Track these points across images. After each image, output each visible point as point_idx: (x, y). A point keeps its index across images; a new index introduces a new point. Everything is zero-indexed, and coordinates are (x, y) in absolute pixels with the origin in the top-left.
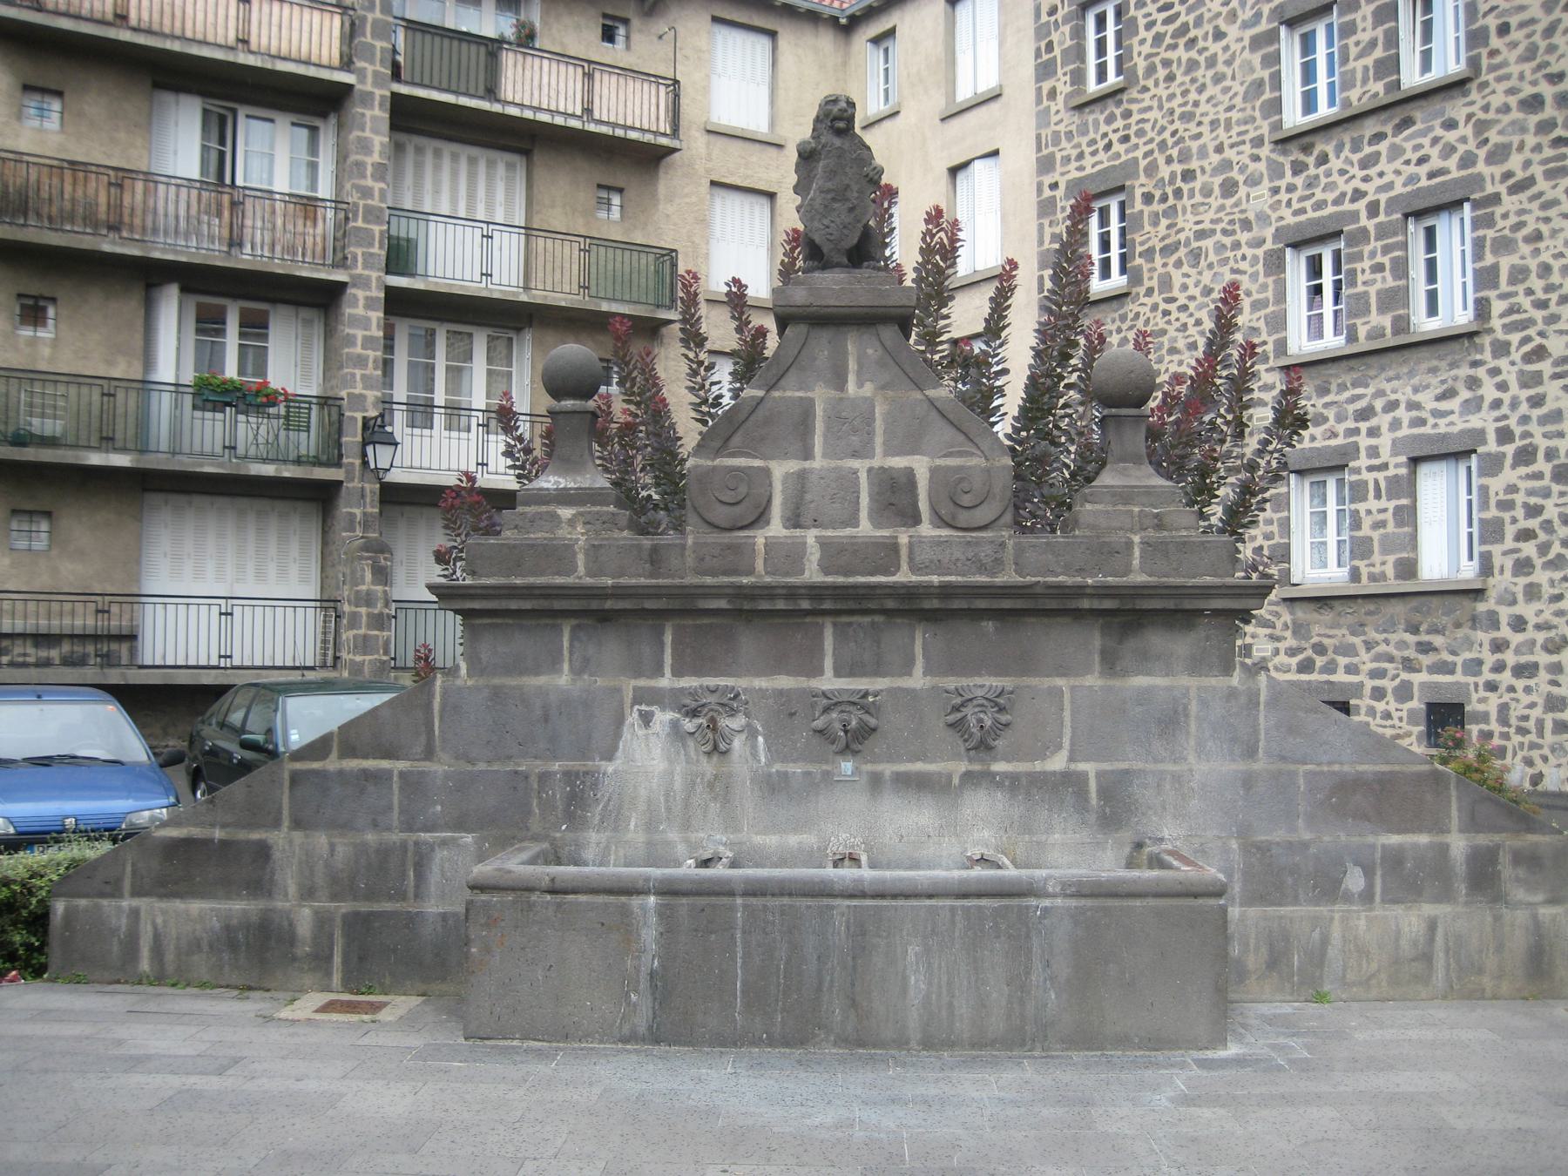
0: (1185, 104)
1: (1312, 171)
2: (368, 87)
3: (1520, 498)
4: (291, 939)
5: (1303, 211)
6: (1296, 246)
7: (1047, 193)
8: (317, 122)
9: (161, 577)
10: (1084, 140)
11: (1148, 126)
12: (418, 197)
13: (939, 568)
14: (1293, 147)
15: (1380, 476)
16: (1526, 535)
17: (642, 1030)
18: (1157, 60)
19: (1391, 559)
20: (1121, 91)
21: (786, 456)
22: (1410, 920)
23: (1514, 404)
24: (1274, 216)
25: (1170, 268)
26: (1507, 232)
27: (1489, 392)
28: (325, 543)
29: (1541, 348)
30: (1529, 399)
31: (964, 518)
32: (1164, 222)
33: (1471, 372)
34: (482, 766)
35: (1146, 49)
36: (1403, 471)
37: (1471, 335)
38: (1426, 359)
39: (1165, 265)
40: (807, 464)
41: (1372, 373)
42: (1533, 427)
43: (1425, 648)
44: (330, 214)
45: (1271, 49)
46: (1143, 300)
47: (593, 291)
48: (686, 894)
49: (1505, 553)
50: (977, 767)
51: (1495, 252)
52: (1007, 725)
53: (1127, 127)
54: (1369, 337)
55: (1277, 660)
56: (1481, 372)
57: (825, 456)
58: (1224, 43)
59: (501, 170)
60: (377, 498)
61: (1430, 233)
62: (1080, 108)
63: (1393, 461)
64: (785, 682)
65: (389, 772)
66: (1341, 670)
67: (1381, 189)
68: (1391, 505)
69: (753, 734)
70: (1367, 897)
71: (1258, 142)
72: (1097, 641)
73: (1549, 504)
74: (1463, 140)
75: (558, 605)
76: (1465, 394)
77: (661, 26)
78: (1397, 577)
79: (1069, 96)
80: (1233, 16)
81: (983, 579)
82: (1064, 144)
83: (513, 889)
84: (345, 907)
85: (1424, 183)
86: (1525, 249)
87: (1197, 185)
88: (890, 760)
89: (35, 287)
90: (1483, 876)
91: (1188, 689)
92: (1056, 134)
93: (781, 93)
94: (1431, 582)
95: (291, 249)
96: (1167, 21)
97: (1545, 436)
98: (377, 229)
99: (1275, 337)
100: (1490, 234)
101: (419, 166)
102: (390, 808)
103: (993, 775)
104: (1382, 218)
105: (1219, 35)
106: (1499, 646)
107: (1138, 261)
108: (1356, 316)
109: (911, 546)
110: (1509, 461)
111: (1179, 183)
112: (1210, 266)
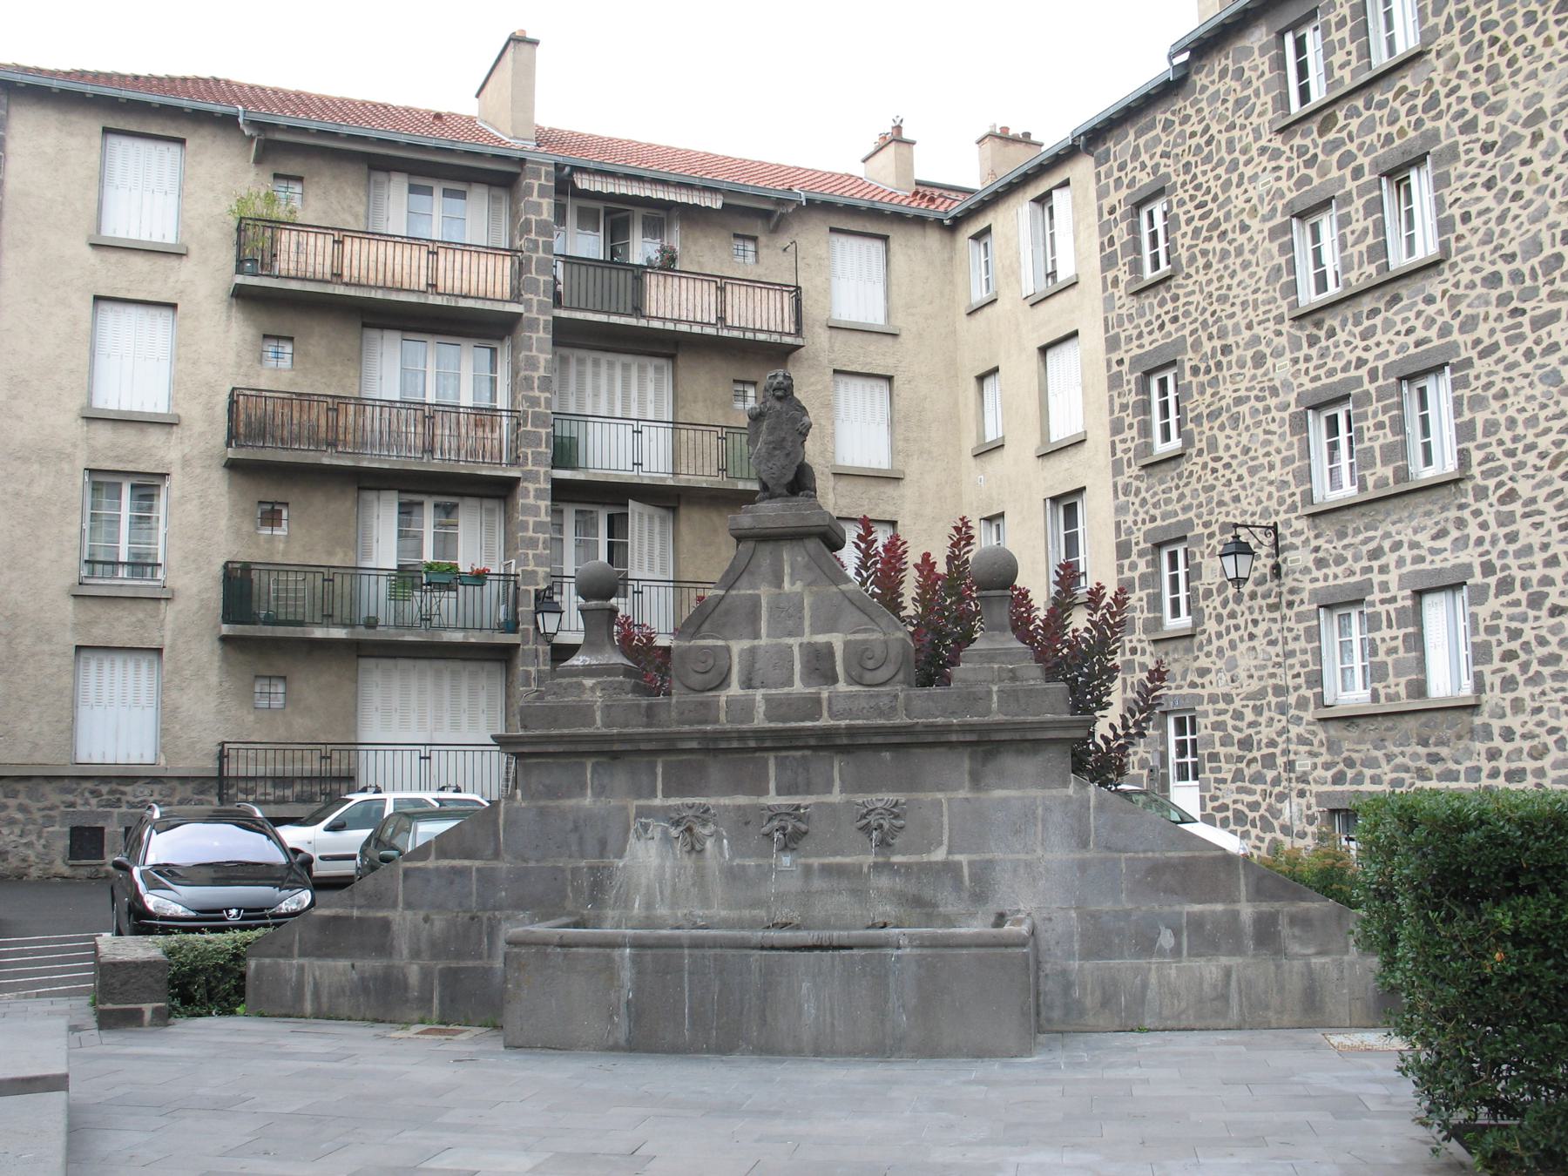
0: (1221, 288)
1: (1323, 343)
2: (534, 315)
5: (1318, 378)
6: (1316, 408)
7: (1115, 368)
8: (495, 344)
9: (373, 728)
10: (1142, 322)
11: (1192, 308)
12: (580, 402)
13: (848, 714)
14: (1307, 322)
15: (1391, 607)
16: (1509, 656)
17: (622, 1041)
18: (1196, 250)
19: (1403, 681)
20: (1170, 278)
21: (741, 637)
22: (1210, 969)
23: (1494, 542)
24: (1295, 383)
25: (1216, 431)
26: (1479, 391)
27: (1473, 531)
28: (508, 696)
29: (1512, 490)
30: (1506, 536)
31: (868, 677)
32: (1209, 391)
33: (1459, 514)
34: (532, 864)
35: (1188, 241)
36: (1409, 603)
37: (1456, 481)
38: (1422, 503)
39: (1211, 429)
40: (756, 642)
41: (1380, 517)
42: (1510, 560)
43: (1434, 758)
44: (505, 421)
46: (1195, 460)
47: (731, 473)
48: (650, 947)
49: (1494, 673)
50: (880, 859)
51: (1471, 409)
53: (1176, 309)
54: (1376, 487)
55: (1315, 774)
56: (1466, 514)
58: (1248, 234)
59: (651, 373)
60: (548, 657)
62: (1137, 293)
63: (1400, 594)
64: (742, 800)
66: (1367, 780)
67: (1378, 357)
68: (1401, 633)
69: (719, 840)
70: (1176, 952)
71: (1279, 319)
72: (966, 764)
73: (1526, 627)
74: (1441, 313)
76: (1455, 534)
77: (784, 240)
78: (1408, 697)
79: (1129, 283)
80: (1254, 210)
82: (1127, 325)
83: (536, 944)
84: (441, 965)
85: (1412, 351)
86: (1495, 405)
87: (1233, 357)
88: (817, 855)
89: (274, 494)
90: (1266, 933)
92: (1120, 316)
93: (894, 288)
95: (473, 453)
96: (1202, 218)
97: (1520, 567)
98: (543, 431)
100: (1467, 393)
101: (581, 375)
104: (1381, 382)
105: (1244, 228)
106: (1493, 755)
107: (1190, 426)
108: (1365, 468)
109: (830, 698)
110: (1492, 591)
111: (1219, 357)
112: (1247, 428)
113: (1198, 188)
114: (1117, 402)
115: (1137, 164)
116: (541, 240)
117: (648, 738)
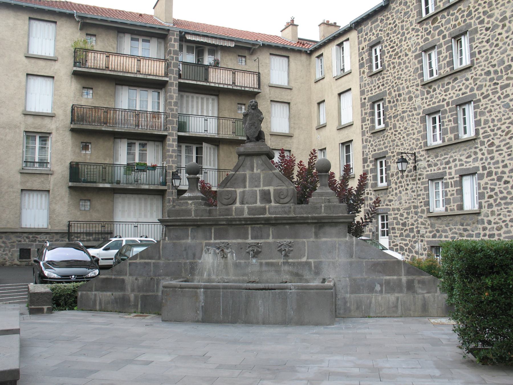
0: (398, 75)
1: (432, 93)
2: (172, 81)
3: (489, 186)
4: (129, 301)
5: (429, 105)
6: (429, 115)
7: (363, 101)
8: (160, 91)
10: (372, 86)
11: (389, 81)
12: (187, 111)
13: (275, 213)
14: (426, 86)
15: (452, 180)
16: (490, 197)
17: (200, 319)
18: (390, 62)
19: (456, 204)
20: (381, 71)
21: (240, 187)
22: (392, 297)
23: (486, 159)
24: (422, 107)
25: (396, 122)
27: (480, 156)
28: (163, 207)
29: (493, 143)
30: (490, 158)
32: (394, 109)
33: (475, 150)
34: (171, 261)
35: (388, 59)
36: (458, 179)
37: (474, 139)
38: (463, 146)
40: (245, 189)
42: (492, 166)
43: (465, 230)
44: (162, 116)
45: (420, 59)
46: (389, 131)
47: (236, 134)
49: (485, 202)
51: (480, 116)
52: (292, 250)
53: (383, 81)
54: (448, 141)
55: (427, 234)
56: (477, 150)
57: (249, 187)
58: (408, 57)
60: (176, 194)
61: (464, 110)
63: (455, 176)
64: (240, 241)
65: (150, 263)
66: (443, 237)
67: (450, 98)
68: (455, 189)
69: (232, 253)
70: (381, 292)
71: (417, 85)
72: (313, 230)
73: (496, 187)
74: (470, 84)
75: (187, 223)
76: (474, 157)
78: (457, 210)
79: (368, 73)
80: (410, 49)
81: (285, 216)
82: (367, 87)
84: (141, 294)
85: (461, 96)
86: (488, 115)
87: (402, 98)
88: (264, 259)
90: (410, 286)
91: (336, 241)
93: (291, 74)
94: (467, 211)
95: (152, 127)
96: (392, 51)
97: (495, 168)
98: (175, 120)
99: (424, 141)
100: (478, 110)
102: (151, 271)
103: (289, 262)
104: (450, 106)
105: (406, 55)
106: (484, 229)
107: (387, 120)
108: (445, 135)
109: (269, 208)
110: (485, 175)
111: (397, 97)
113: (391, 41)
114: (364, 112)
115: (371, 33)
116: (175, 56)
117: (209, 220)
